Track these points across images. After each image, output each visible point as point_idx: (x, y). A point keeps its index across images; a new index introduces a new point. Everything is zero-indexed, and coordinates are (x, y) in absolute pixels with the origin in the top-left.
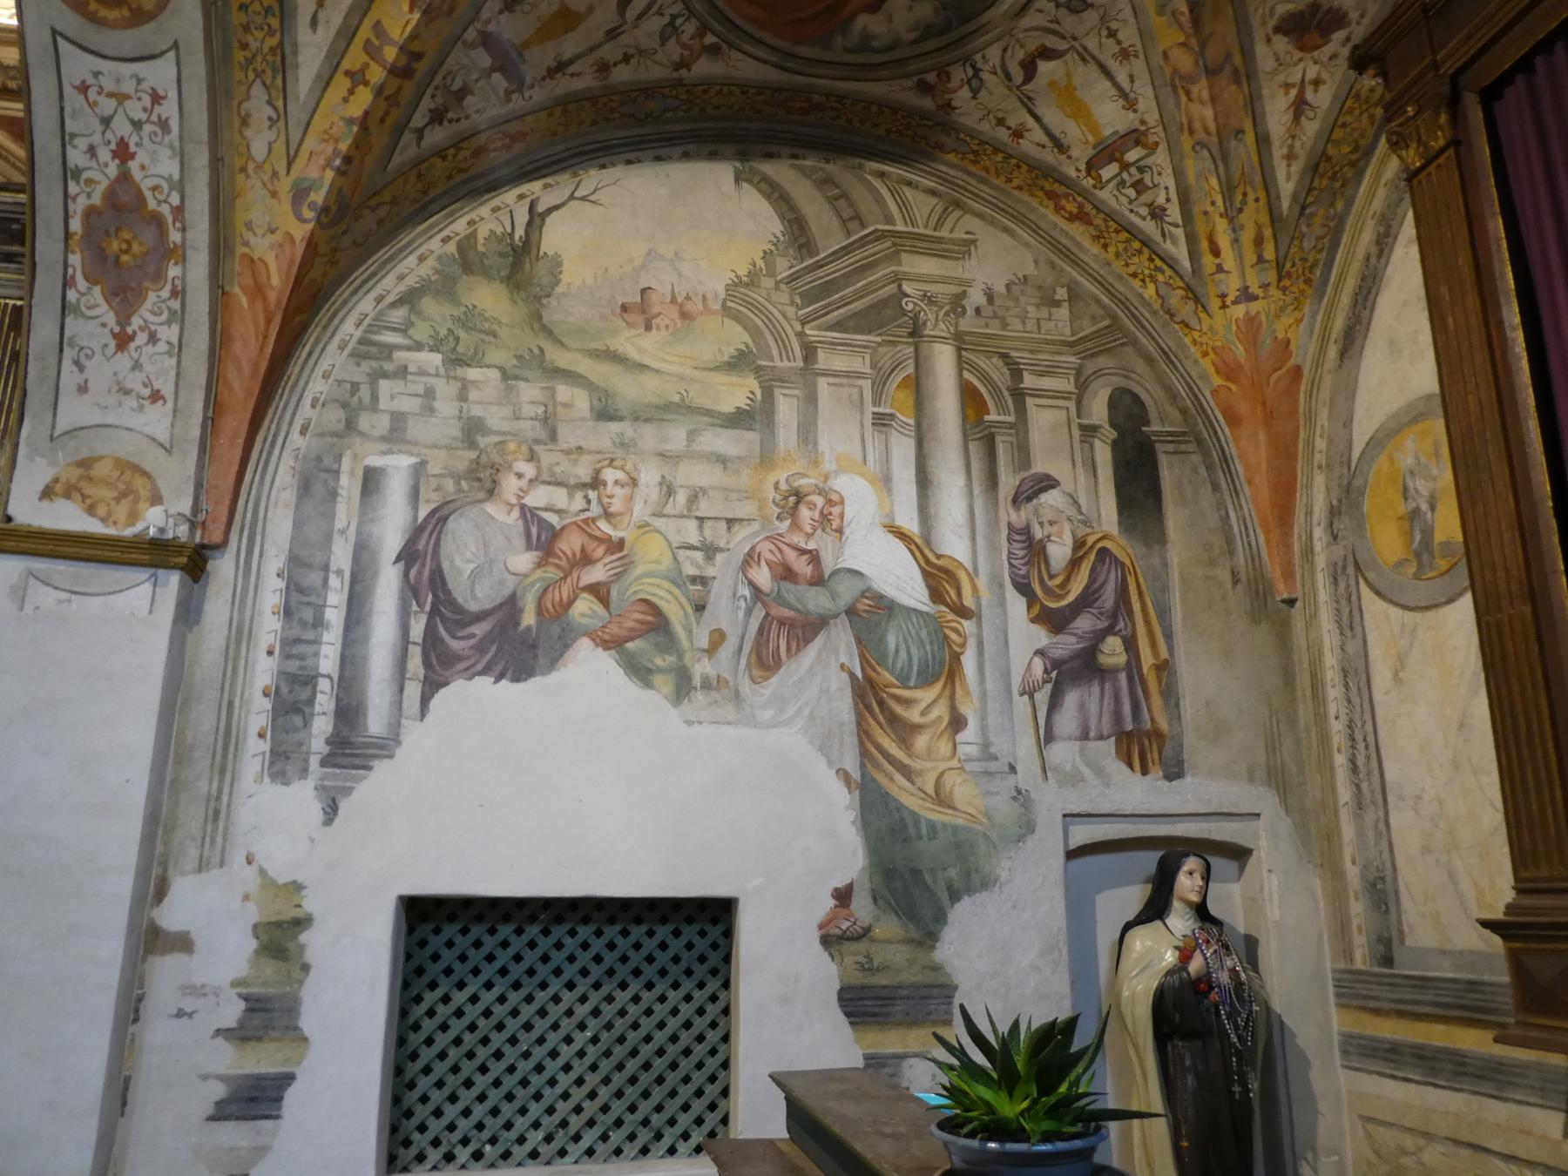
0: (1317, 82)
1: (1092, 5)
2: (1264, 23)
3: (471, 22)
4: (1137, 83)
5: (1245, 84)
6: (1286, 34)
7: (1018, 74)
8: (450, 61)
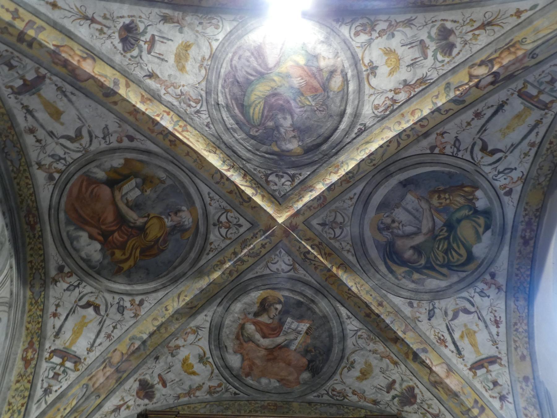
0: (128, 407)
1: (123, 315)
2: (140, 375)
3: (49, 71)
4: (99, 347)
5: (117, 384)
6: (140, 384)
7: (83, 302)
8: (28, 61)
